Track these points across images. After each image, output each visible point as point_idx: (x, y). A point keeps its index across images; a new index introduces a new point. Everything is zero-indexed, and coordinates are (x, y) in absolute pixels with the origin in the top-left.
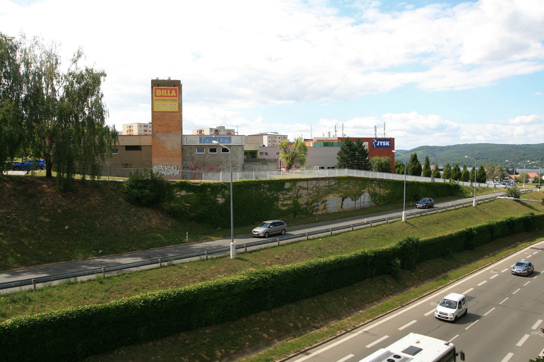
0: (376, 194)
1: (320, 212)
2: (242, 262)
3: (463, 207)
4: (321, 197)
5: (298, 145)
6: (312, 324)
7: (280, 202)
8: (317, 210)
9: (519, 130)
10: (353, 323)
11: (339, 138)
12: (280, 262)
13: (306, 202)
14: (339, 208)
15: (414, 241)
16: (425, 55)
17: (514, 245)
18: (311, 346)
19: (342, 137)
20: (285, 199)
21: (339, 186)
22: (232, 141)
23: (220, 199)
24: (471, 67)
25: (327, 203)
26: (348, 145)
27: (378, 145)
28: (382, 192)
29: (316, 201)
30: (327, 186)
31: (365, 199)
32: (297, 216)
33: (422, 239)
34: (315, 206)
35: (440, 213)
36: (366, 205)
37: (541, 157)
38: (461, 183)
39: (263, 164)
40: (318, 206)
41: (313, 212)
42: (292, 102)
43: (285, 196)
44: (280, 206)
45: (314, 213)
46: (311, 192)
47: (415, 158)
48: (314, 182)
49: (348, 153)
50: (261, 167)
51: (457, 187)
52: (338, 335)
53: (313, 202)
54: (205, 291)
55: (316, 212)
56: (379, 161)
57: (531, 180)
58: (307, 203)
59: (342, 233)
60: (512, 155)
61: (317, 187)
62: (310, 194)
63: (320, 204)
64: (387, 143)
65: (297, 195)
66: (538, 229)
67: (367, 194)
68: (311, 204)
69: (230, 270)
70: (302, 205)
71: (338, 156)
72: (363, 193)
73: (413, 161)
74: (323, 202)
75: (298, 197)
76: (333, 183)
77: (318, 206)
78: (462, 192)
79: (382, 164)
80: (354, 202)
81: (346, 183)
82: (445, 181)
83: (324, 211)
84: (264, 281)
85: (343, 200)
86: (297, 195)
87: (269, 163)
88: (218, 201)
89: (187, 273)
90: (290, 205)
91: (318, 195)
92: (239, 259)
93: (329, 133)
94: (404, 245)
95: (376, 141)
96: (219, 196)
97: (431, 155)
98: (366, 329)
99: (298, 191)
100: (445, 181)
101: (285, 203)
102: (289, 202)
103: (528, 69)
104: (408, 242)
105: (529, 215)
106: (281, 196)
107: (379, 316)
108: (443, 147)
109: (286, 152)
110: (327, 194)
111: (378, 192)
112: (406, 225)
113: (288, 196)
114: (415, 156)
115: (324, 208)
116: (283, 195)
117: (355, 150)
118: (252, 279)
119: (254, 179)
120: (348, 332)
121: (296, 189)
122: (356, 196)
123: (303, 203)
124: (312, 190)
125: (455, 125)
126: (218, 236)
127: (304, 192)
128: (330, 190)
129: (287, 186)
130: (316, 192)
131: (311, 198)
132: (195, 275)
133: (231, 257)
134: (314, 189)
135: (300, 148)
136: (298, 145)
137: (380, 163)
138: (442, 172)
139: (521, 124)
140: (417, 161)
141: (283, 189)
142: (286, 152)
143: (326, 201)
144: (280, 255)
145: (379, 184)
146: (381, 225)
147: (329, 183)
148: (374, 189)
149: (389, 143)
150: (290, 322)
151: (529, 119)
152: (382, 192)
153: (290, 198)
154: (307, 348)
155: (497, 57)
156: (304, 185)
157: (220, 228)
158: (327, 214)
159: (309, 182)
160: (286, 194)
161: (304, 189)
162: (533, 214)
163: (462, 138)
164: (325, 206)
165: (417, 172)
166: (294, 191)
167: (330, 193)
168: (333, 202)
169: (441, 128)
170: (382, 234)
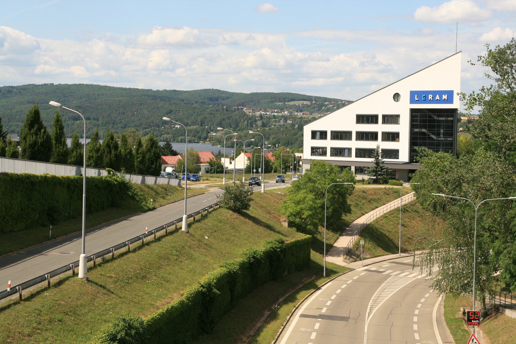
3: (167, 234)
9: (157, 58)
15: (136, 329)
17: (267, 313)
35: (134, 251)
37: (199, 119)
38: (135, 179)
47: (35, 121)
51: (124, 186)
60: (145, 111)
66: (286, 273)
78: (133, 198)
82: (99, 174)
100: (99, 174)
105: (278, 245)
112: (91, 288)
114: (36, 114)
125: (25, 38)
138: (20, 149)
139: (164, 45)
140: (41, 127)
146: (38, 293)
151: (178, 35)
162: (282, 242)
163: (38, 70)
165: (39, 153)
170: (59, 316)
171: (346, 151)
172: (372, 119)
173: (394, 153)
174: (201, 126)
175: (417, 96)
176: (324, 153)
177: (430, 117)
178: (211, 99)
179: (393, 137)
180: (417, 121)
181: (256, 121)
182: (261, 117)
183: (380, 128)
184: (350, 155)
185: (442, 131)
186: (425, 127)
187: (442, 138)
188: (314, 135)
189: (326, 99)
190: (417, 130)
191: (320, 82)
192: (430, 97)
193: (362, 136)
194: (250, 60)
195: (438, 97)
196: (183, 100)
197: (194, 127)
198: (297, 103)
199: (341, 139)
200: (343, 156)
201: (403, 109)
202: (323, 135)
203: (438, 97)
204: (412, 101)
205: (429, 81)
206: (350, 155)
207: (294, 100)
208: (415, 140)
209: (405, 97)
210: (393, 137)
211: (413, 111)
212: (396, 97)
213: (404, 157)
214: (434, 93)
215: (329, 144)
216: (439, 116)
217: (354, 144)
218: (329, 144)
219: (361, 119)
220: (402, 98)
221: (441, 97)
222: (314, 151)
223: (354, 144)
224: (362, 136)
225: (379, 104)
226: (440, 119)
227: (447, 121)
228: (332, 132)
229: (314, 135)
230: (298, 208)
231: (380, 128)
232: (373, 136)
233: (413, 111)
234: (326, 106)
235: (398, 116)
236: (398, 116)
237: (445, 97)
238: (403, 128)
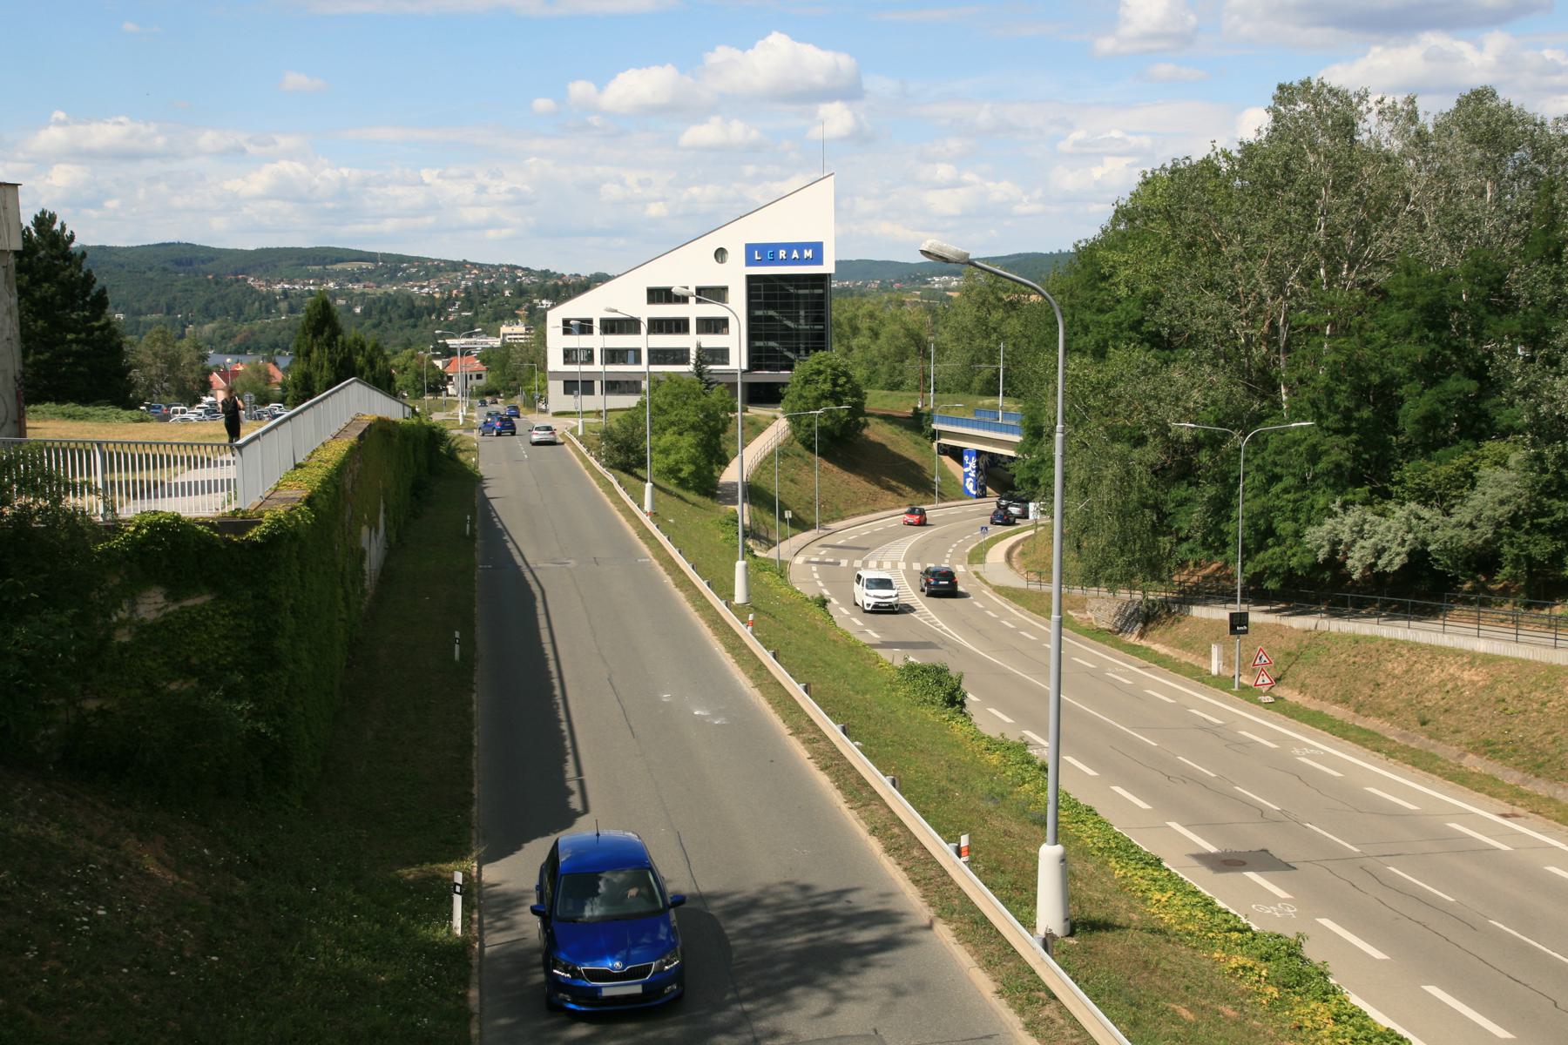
37: (163, 300)
139: (79, 155)
151: (107, 133)
171: (631, 354)
173: (721, 355)
174: (168, 313)
175: (758, 252)
176: (590, 358)
177: (782, 289)
178: (178, 263)
180: (758, 297)
181: (276, 302)
182: (285, 293)
184: (638, 361)
185: (802, 313)
186: (774, 308)
187: (803, 325)
189: (402, 259)
190: (759, 313)
191: (389, 225)
192: (782, 254)
193: (658, 326)
194: (258, 181)
195: (795, 254)
196: (122, 266)
197: (155, 317)
198: (349, 266)
200: (625, 362)
202: (585, 327)
203: (795, 254)
204: (750, 261)
206: (638, 361)
207: (342, 261)
209: (737, 256)
211: (751, 279)
212: (720, 254)
213: (738, 360)
214: (789, 247)
215: (598, 341)
216: (797, 287)
217: (644, 341)
219: (659, 295)
220: (730, 257)
221: (801, 253)
222: (569, 355)
223: (644, 341)
224: (658, 326)
226: (801, 292)
227: (812, 296)
228: (602, 321)
229: (567, 327)
231: (693, 311)
232: (680, 326)
233: (751, 279)
234: (404, 270)
235: (725, 289)
236: (725, 289)
237: (808, 253)
238: (736, 308)
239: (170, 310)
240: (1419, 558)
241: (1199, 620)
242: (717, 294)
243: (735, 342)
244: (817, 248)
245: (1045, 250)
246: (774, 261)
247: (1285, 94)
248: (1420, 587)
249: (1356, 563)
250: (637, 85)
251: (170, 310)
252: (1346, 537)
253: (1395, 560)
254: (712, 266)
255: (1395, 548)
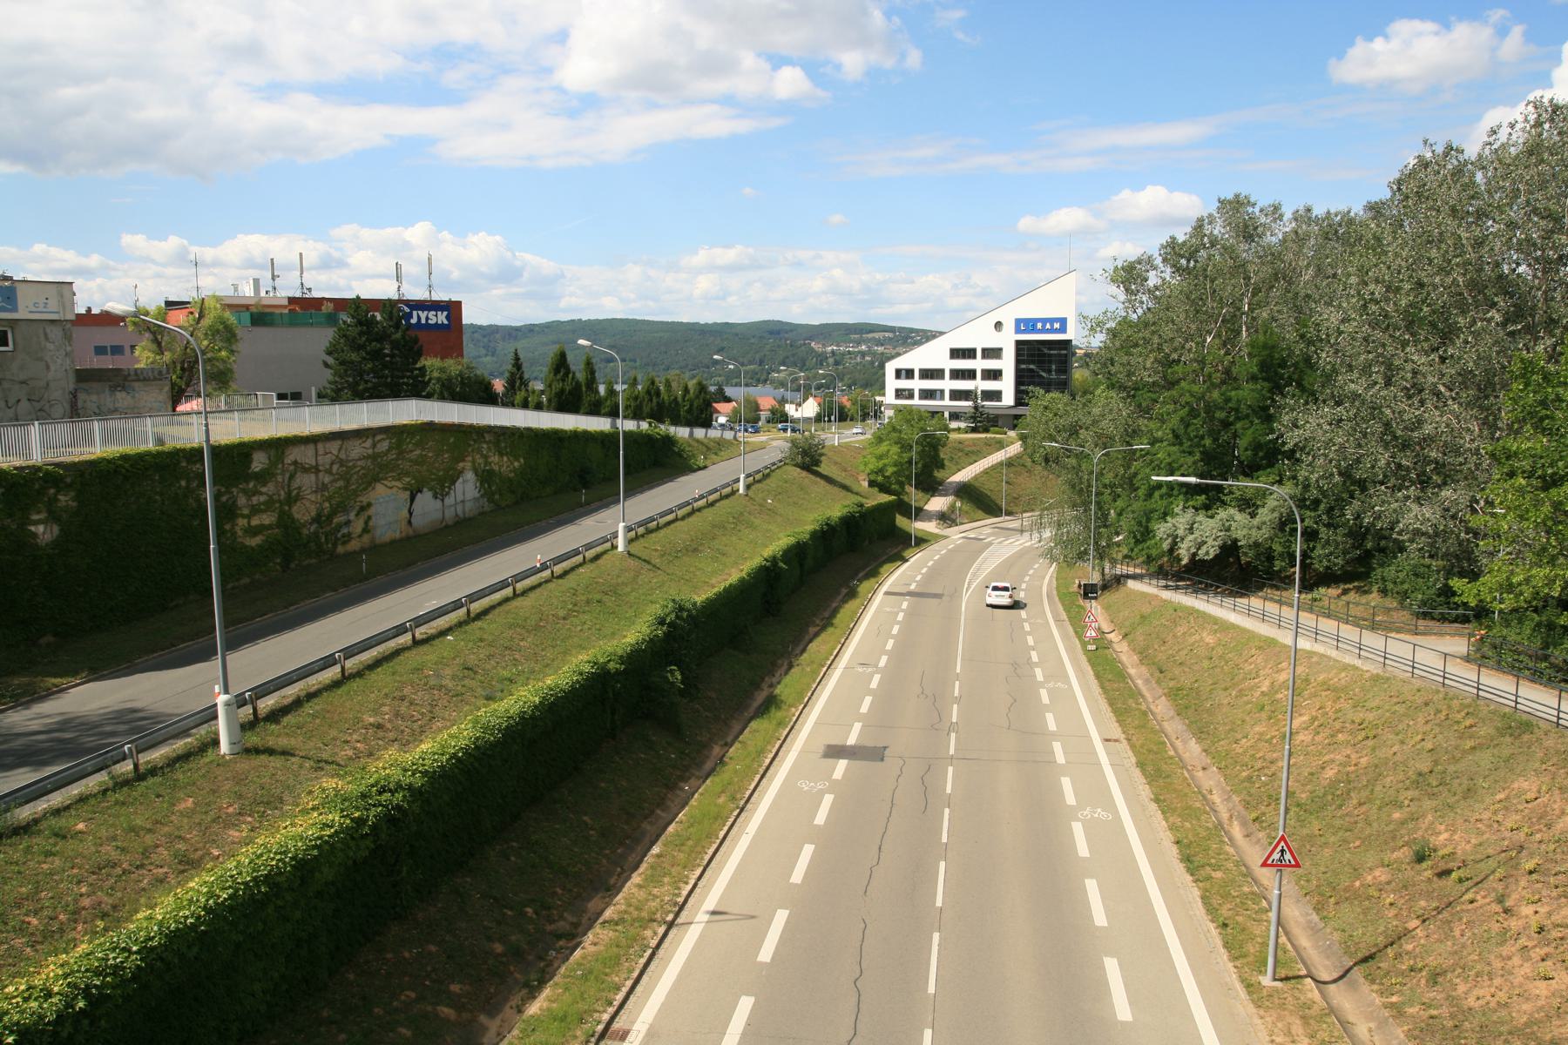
0: (491, 473)
1: (354, 545)
2: (276, 762)
4: (356, 493)
5: (206, 322)
6: (549, 928)
7: (242, 522)
8: (348, 538)
9: (704, 283)
10: (664, 891)
11: (292, 300)
12: (391, 735)
13: (313, 514)
14: (404, 523)
16: (446, 54)
18: (610, 1004)
19: (298, 295)
20: (255, 510)
21: (401, 453)
22: (21, 303)
23: (41, 528)
24: (586, 104)
25: (371, 511)
26: (360, 323)
27: (414, 321)
28: (505, 465)
29: (341, 508)
30: (369, 457)
31: (467, 489)
32: (293, 566)
33: (700, 598)
34: (340, 526)
35: (683, 518)
36: (470, 509)
37: (758, 357)
38: (682, 432)
39: (114, 388)
40: (348, 523)
41: (335, 545)
42: (18, 169)
43: (255, 500)
44: (240, 533)
45: (340, 549)
46: (327, 479)
48: (334, 447)
49: (361, 347)
50: (107, 400)
51: (669, 441)
52: (653, 943)
53: (334, 513)
54: (231, 909)
55: (344, 543)
56: (442, 370)
57: (764, 415)
58: (317, 519)
59: (493, 607)
61: (342, 463)
62: (324, 487)
63: (352, 516)
64: (442, 318)
65: (289, 493)
67: (470, 475)
68: (330, 517)
69: (256, 802)
70: (304, 525)
71: (330, 360)
72: (461, 472)
73: (557, 370)
74: (362, 509)
75: (292, 499)
76: (384, 446)
77: (348, 523)
79: (449, 379)
80: (438, 503)
81: (416, 445)
83: (366, 539)
84: (393, 819)
85: (412, 499)
86: (289, 493)
87: (136, 384)
88: (35, 535)
89: (109, 851)
90: (270, 527)
91: (346, 487)
92: (257, 751)
93: (256, 282)
94: (670, 625)
95: (407, 310)
96: (35, 517)
97: (483, 351)
98: (711, 902)
99: (292, 477)
101: (255, 522)
102: (267, 519)
103: (715, 125)
104: (677, 617)
106: (242, 501)
107: (711, 851)
108: (517, 329)
109: (159, 344)
110: (370, 484)
111: (496, 468)
112: (632, 562)
113: (263, 499)
115: (366, 530)
116: (250, 494)
117: (382, 337)
118: (360, 822)
119: (151, 446)
120: (671, 925)
121: (283, 474)
122: (443, 485)
123: (307, 518)
124: (329, 472)
125: (547, 266)
126: (75, 673)
127: (306, 481)
128: (377, 471)
129: (259, 462)
130: (341, 477)
131: (329, 499)
132: (146, 853)
133: (224, 747)
134: (335, 467)
135: (213, 332)
136: (206, 322)
137: (444, 376)
139: (712, 268)
141: (248, 477)
142: (159, 344)
143: (369, 505)
144: (376, 712)
145: (497, 444)
147: (374, 446)
148: (486, 457)
149: (447, 317)
150: (490, 939)
151: (730, 255)
152: (505, 465)
153: (269, 505)
154: (606, 1017)
155: (652, 82)
156: (305, 455)
157: (49, 639)
158: (375, 549)
159: (320, 446)
160: (256, 492)
161: (306, 470)
163: (563, 303)
164: (366, 523)
166: (280, 478)
167: (377, 479)
168: (389, 510)
169: (508, 274)
172: (969, 353)
173: (996, 395)
175: (1024, 324)
178: (771, 333)
179: (995, 375)
182: (833, 352)
183: (979, 364)
184: (942, 398)
186: (1033, 362)
188: (898, 374)
189: (912, 330)
192: (1039, 326)
193: (957, 374)
198: (876, 335)
199: (932, 378)
201: (1007, 342)
202: (909, 374)
204: (1018, 331)
205: (1036, 306)
206: (942, 398)
208: (1021, 378)
209: (1009, 326)
210: (995, 375)
211: (1018, 343)
212: (998, 325)
213: (1008, 399)
214: (1044, 321)
215: (917, 384)
217: (948, 385)
218: (917, 384)
219: (956, 353)
222: (899, 393)
223: (948, 385)
224: (957, 374)
225: (977, 335)
229: (898, 374)
230: (880, 464)
231: (979, 364)
232: (970, 374)
233: (1018, 343)
235: (1001, 349)
236: (1001, 349)
237: (1057, 326)
238: (1007, 364)
239: (761, 363)
240: (1230, 549)
241: (1133, 592)
242: (992, 353)
243: (1007, 387)
244: (1063, 321)
245: (685, 318)
246: (1034, 330)
247: (1234, 207)
248: (1232, 572)
249: (1184, 553)
250: (1067, 218)
251: (761, 363)
252: (1180, 532)
253: (1210, 551)
254: (995, 333)
255: (1210, 542)
